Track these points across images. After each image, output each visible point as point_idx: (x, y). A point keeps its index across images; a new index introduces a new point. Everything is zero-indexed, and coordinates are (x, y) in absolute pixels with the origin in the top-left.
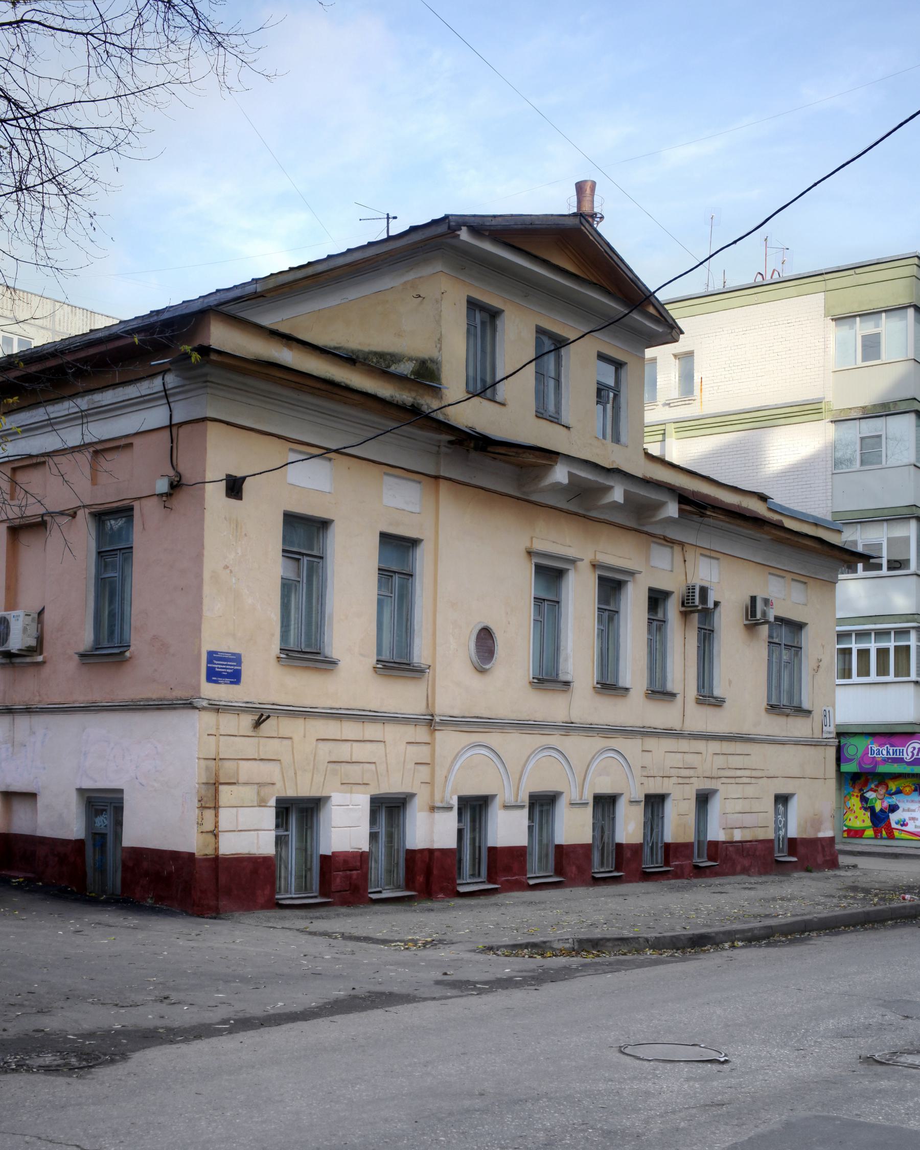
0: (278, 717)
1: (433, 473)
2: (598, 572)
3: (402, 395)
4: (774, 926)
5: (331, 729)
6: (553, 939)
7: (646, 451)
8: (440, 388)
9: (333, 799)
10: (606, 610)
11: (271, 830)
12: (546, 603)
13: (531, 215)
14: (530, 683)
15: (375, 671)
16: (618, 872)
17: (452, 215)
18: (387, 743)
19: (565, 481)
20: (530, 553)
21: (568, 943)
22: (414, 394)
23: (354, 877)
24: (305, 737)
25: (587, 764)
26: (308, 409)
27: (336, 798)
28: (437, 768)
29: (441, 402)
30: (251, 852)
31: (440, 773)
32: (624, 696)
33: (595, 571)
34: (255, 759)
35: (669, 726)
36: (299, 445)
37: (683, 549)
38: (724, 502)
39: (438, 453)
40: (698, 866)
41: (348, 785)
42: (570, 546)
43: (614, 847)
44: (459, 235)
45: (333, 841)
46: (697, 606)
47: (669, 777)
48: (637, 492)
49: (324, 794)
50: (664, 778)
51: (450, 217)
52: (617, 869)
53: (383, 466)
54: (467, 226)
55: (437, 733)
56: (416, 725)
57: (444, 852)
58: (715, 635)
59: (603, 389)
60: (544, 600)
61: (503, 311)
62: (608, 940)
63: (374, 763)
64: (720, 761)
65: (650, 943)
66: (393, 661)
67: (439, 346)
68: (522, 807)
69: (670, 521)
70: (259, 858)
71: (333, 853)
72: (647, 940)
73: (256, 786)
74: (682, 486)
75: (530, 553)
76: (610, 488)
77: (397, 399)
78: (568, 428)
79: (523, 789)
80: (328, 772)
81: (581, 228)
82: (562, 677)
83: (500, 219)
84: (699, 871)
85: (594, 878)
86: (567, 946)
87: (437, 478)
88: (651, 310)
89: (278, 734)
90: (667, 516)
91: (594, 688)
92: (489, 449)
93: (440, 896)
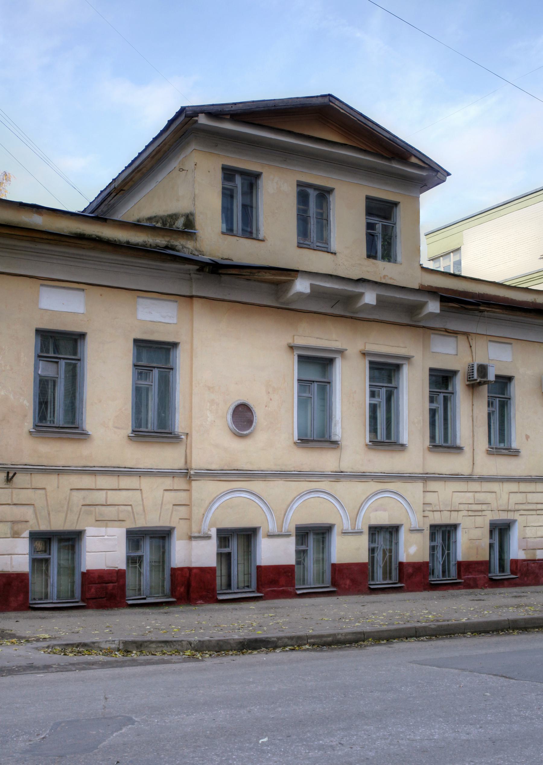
0: (31, 474)
1: (188, 294)
2: (296, 353)
3: (156, 240)
4: (366, 632)
5: (86, 481)
6: (101, 640)
7: (422, 266)
8: (195, 233)
9: (87, 532)
10: (383, 386)
11: (25, 554)
12: (316, 384)
13: (274, 100)
14: (295, 443)
15: (130, 438)
16: (401, 584)
17: (188, 107)
18: (143, 491)
19: (308, 290)
20: (292, 348)
21: (115, 644)
22: (167, 239)
23: (110, 588)
24: (58, 487)
25: (361, 502)
26: (76, 258)
27: (90, 531)
28: (194, 508)
29: (195, 242)
30: (4, 571)
31: (197, 512)
32: (403, 451)
33: (365, 358)
34: (9, 504)
35: (456, 472)
36: (50, 282)
37: (468, 338)
38: (515, 300)
39: (191, 279)
40: (492, 578)
41: (102, 521)
42: (336, 341)
43: (398, 565)
44: (197, 121)
45: (87, 562)
46: (476, 380)
47: (458, 511)
48: (392, 295)
49: (78, 528)
50: (434, 512)
51: (187, 108)
52: (400, 581)
53: (81, 284)
54: (205, 113)
55: (193, 483)
56: (173, 477)
57: (203, 570)
58: (512, 401)
59: (377, 223)
60: (314, 381)
61: (262, 173)
62: (152, 642)
63: (131, 505)
64: (520, 498)
65: (192, 645)
66: (153, 431)
67: (194, 202)
68: (288, 536)
69: (432, 315)
70: (13, 574)
71: (88, 571)
72: (190, 643)
73: (9, 524)
74: (466, 290)
75: (292, 348)
76: (361, 295)
77: (149, 243)
78: (335, 254)
79: (288, 521)
80: (81, 513)
81: (330, 105)
82: (334, 438)
83: (241, 105)
84: (495, 583)
85: (370, 588)
86: (113, 646)
87: (191, 297)
88: (413, 160)
89: (31, 486)
90: (428, 312)
91: (367, 445)
92: (220, 271)
93: (199, 602)
